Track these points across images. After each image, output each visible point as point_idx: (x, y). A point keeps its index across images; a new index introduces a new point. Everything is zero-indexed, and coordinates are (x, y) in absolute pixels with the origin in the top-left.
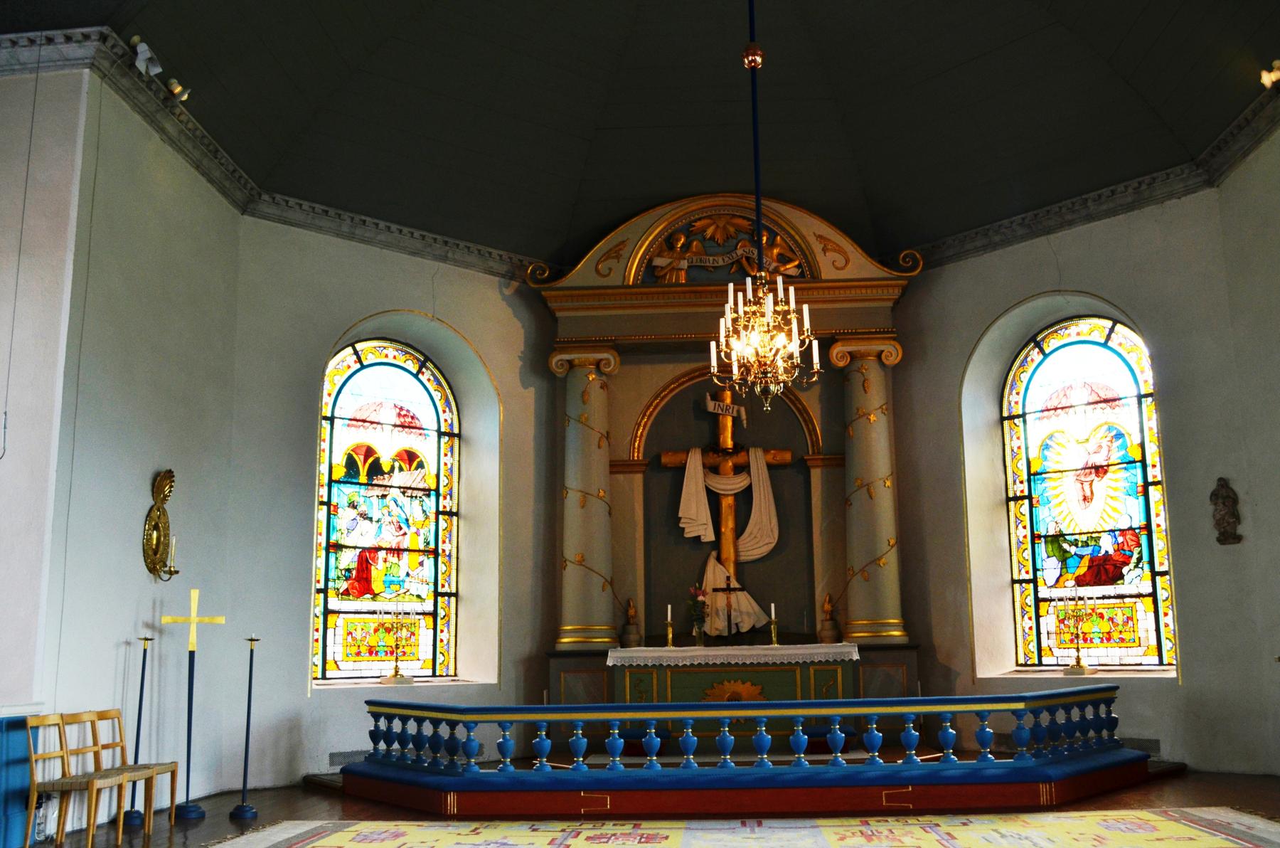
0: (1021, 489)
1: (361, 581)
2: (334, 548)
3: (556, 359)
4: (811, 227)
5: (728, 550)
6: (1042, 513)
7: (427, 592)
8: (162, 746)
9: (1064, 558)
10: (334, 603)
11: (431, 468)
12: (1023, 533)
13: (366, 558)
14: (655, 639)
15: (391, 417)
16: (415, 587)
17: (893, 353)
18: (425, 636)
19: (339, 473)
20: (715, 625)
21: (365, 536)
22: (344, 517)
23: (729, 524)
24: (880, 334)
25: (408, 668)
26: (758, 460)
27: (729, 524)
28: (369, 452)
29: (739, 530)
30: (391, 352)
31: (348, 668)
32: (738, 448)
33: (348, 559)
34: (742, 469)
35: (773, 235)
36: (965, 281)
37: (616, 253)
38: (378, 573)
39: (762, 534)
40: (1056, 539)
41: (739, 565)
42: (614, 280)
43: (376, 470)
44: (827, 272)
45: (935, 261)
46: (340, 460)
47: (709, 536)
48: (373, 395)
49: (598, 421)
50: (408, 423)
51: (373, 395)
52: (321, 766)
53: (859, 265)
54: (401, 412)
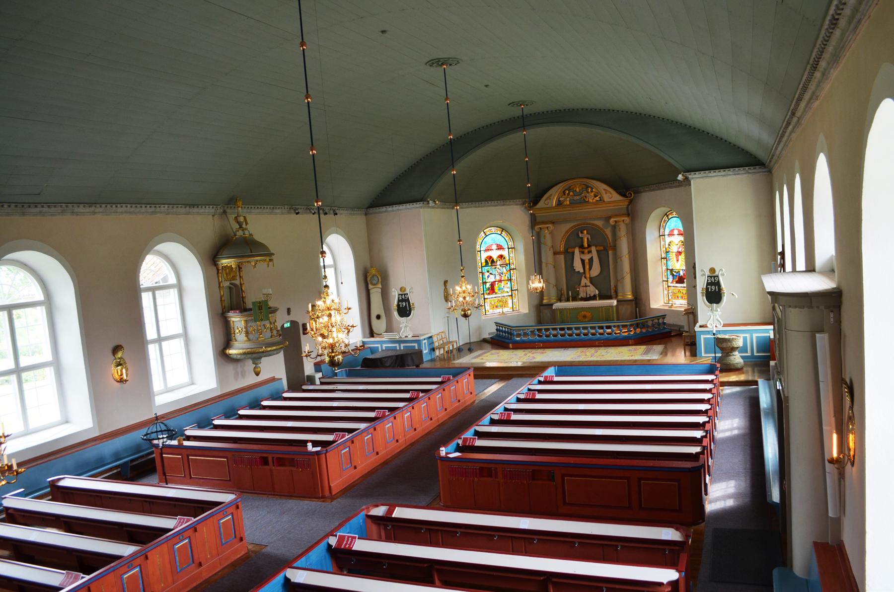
0: (663, 256)
1: (492, 290)
2: (484, 283)
3: (537, 227)
4: (602, 187)
5: (588, 276)
6: (669, 263)
7: (509, 290)
8: (454, 337)
9: (673, 275)
10: (486, 296)
11: (507, 258)
12: (664, 268)
13: (493, 284)
14: (568, 300)
15: (494, 247)
16: (506, 290)
17: (627, 219)
18: (510, 301)
19: (484, 264)
20: (582, 295)
21: (492, 279)
22: (487, 274)
23: (587, 267)
24: (623, 215)
25: (505, 310)
26: (593, 249)
27: (587, 267)
28: (491, 257)
29: (590, 269)
30: (493, 229)
31: (491, 311)
32: (589, 246)
33: (488, 285)
34: (590, 252)
35: (592, 189)
36: (646, 198)
37: (549, 198)
38: (496, 287)
39: (596, 270)
40: (672, 270)
41: (590, 278)
42: (549, 205)
43: (493, 261)
44: (606, 199)
45: (637, 192)
46: (483, 261)
47: (582, 271)
48: (491, 242)
49: (549, 244)
50: (500, 247)
51: (491, 242)
52: (487, 336)
53: (616, 197)
54: (498, 245)
